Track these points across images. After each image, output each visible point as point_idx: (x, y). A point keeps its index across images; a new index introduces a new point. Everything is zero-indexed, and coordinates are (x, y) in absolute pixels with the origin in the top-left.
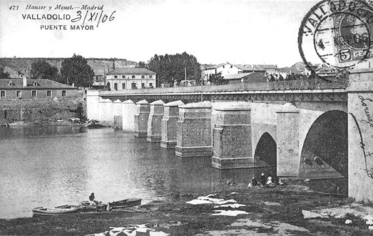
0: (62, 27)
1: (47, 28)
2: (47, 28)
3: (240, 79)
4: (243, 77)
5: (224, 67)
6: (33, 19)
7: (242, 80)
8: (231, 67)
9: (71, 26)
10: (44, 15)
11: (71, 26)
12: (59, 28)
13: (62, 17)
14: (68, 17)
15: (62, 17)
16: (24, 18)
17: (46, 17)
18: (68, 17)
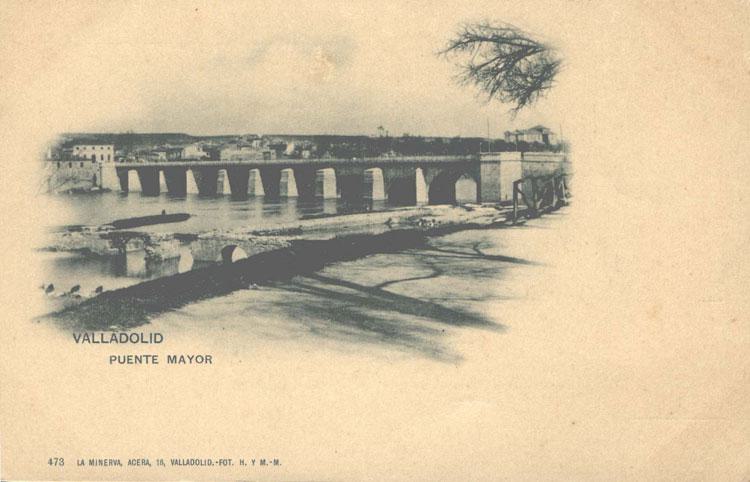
0: (150, 359)
1: (122, 360)
2: (122, 360)
9: (169, 356)
11: (169, 356)
14: (158, 338)
16: (77, 341)
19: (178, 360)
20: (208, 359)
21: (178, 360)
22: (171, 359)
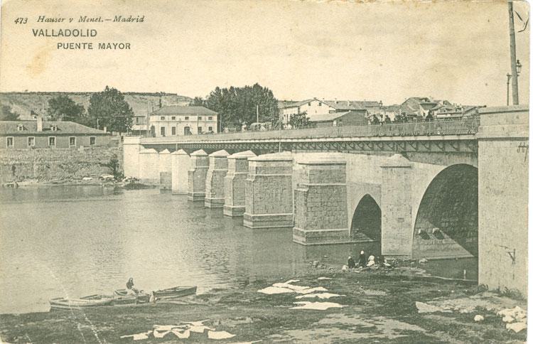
0: (87, 46)
1: (66, 47)
2: (66, 47)
3: (332, 121)
4: (335, 119)
5: (309, 105)
6: (47, 35)
7: (335, 123)
8: (320, 104)
9: (100, 44)
10: (61, 30)
12: (82, 46)
13: (85, 33)
15: (85, 33)
16: (35, 35)
17: (64, 34)
18: (94, 33)
19: (106, 47)
20: (128, 46)
21: (106, 47)
22: (102, 46)
